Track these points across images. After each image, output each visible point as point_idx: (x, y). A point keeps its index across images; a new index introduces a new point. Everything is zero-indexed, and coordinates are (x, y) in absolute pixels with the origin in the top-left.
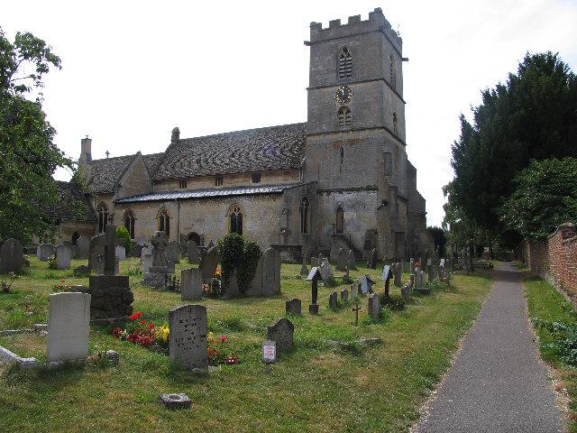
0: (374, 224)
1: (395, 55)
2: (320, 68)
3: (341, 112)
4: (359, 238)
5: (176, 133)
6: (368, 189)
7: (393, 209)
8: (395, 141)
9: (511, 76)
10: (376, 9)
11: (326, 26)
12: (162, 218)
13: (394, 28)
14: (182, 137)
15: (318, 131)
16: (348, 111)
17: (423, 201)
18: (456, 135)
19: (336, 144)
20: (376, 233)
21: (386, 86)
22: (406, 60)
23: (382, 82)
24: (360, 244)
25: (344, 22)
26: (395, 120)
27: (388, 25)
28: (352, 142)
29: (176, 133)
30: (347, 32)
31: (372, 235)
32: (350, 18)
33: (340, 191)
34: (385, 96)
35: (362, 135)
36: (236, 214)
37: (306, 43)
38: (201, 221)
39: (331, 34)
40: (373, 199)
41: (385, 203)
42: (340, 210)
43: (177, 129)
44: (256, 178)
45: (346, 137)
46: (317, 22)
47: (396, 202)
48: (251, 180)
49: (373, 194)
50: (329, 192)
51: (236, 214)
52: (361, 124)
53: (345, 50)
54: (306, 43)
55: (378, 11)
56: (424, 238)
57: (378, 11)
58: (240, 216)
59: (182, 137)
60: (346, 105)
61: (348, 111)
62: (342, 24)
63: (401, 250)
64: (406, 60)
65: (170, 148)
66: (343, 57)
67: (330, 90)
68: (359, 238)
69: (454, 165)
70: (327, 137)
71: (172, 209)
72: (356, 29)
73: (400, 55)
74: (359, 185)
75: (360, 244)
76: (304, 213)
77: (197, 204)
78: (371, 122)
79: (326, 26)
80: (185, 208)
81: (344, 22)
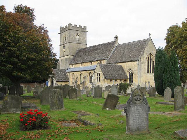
22: (87, 32)
64: (87, 32)
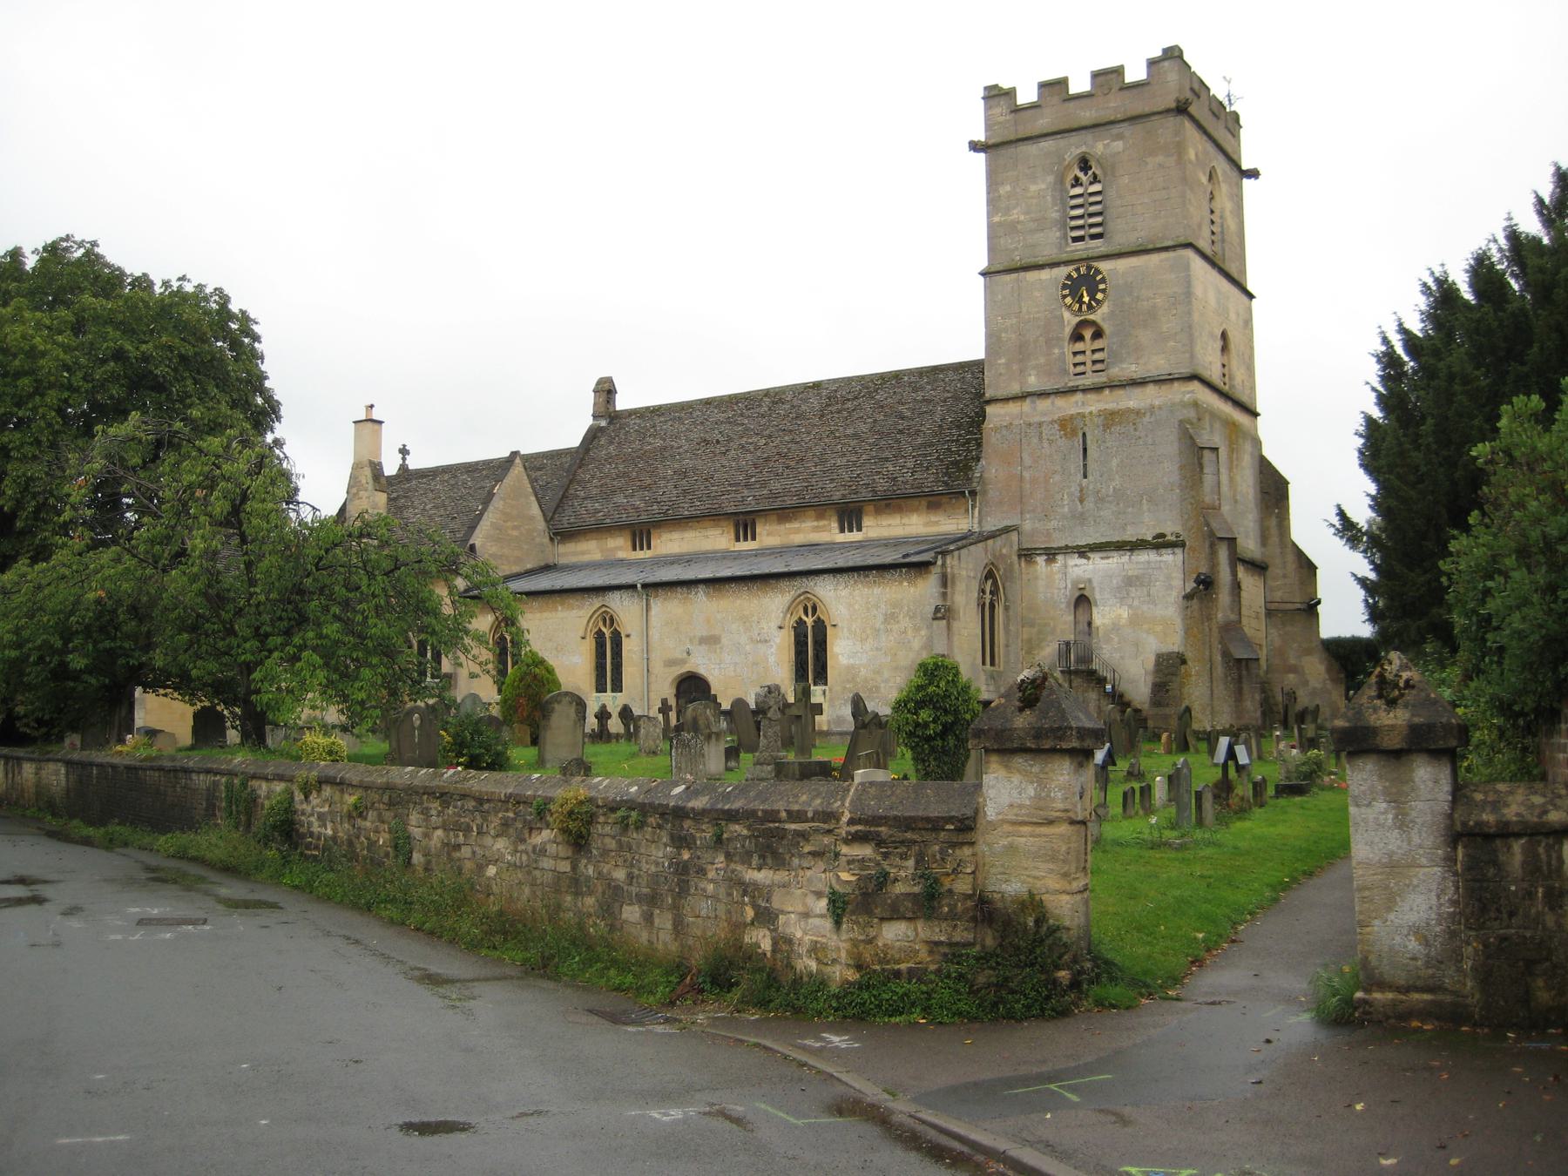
0: (1174, 642)
1: (1221, 165)
2: (1016, 214)
3: (1077, 337)
4: (1136, 676)
5: (606, 390)
6: (1160, 543)
7: (1224, 596)
8: (1227, 409)
9: (1371, 570)
10: (1165, 51)
11: (1027, 95)
12: (600, 636)
13: (1218, 90)
14: (623, 403)
15: (1015, 389)
16: (1098, 334)
17: (1287, 483)
18: (1368, 501)
19: (1067, 426)
20: (1184, 662)
21: (1198, 264)
22: (1253, 174)
23: (1189, 253)
24: (1139, 689)
25: (1080, 84)
26: (1225, 348)
27: (1199, 88)
28: (1111, 419)
29: (606, 390)
30: (1087, 115)
31: (1169, 668)
32: (1096, 75)
33: (1083, 551)
34: (1198, 290)
35: (1132, 400)
36: (809, 621)
37: (975, 147)
38: (711, 641)
39: (1043, 122)
40: (1170, 572)
41: (1206, 584)
42: (1082, 601)
43: (610, 380)
44: (850, 516)
45: (1093, 405)
46: (1005, 85)
47: (1234, 573)
48: (835, 525)
49: (1171, 558)
50: (1051, 554)
51: (809, 621)
52: (1131, 369)
53: (1085, 165)
54: (975, 147)
55: (1173, 54)
56: (1316, 670)
57: (1173, 54)
58: (820, 628)
59: (623, 403)
60: (1091, 317)
61: (1098, 334)
62: (1074, 89)
63: (1252, 705)
64: (1253, 174)
65: (592, 436)
66: (1077, 182)
67: (1045, 274)
68: (1136, 676)
69: (1443, 296)
70: (1044, 405)
71: (626, 610)
72: (1115, 106)
73: (1235, 164)
74: (1130, 535)
75: (1139, 689)
76: (988, 612)
77: (700, 597)
78: (1158, 364)
79: (1027, 95)
80: (664, 608)
81: (1080, 84)
